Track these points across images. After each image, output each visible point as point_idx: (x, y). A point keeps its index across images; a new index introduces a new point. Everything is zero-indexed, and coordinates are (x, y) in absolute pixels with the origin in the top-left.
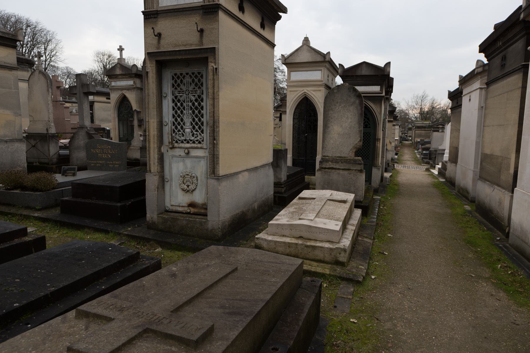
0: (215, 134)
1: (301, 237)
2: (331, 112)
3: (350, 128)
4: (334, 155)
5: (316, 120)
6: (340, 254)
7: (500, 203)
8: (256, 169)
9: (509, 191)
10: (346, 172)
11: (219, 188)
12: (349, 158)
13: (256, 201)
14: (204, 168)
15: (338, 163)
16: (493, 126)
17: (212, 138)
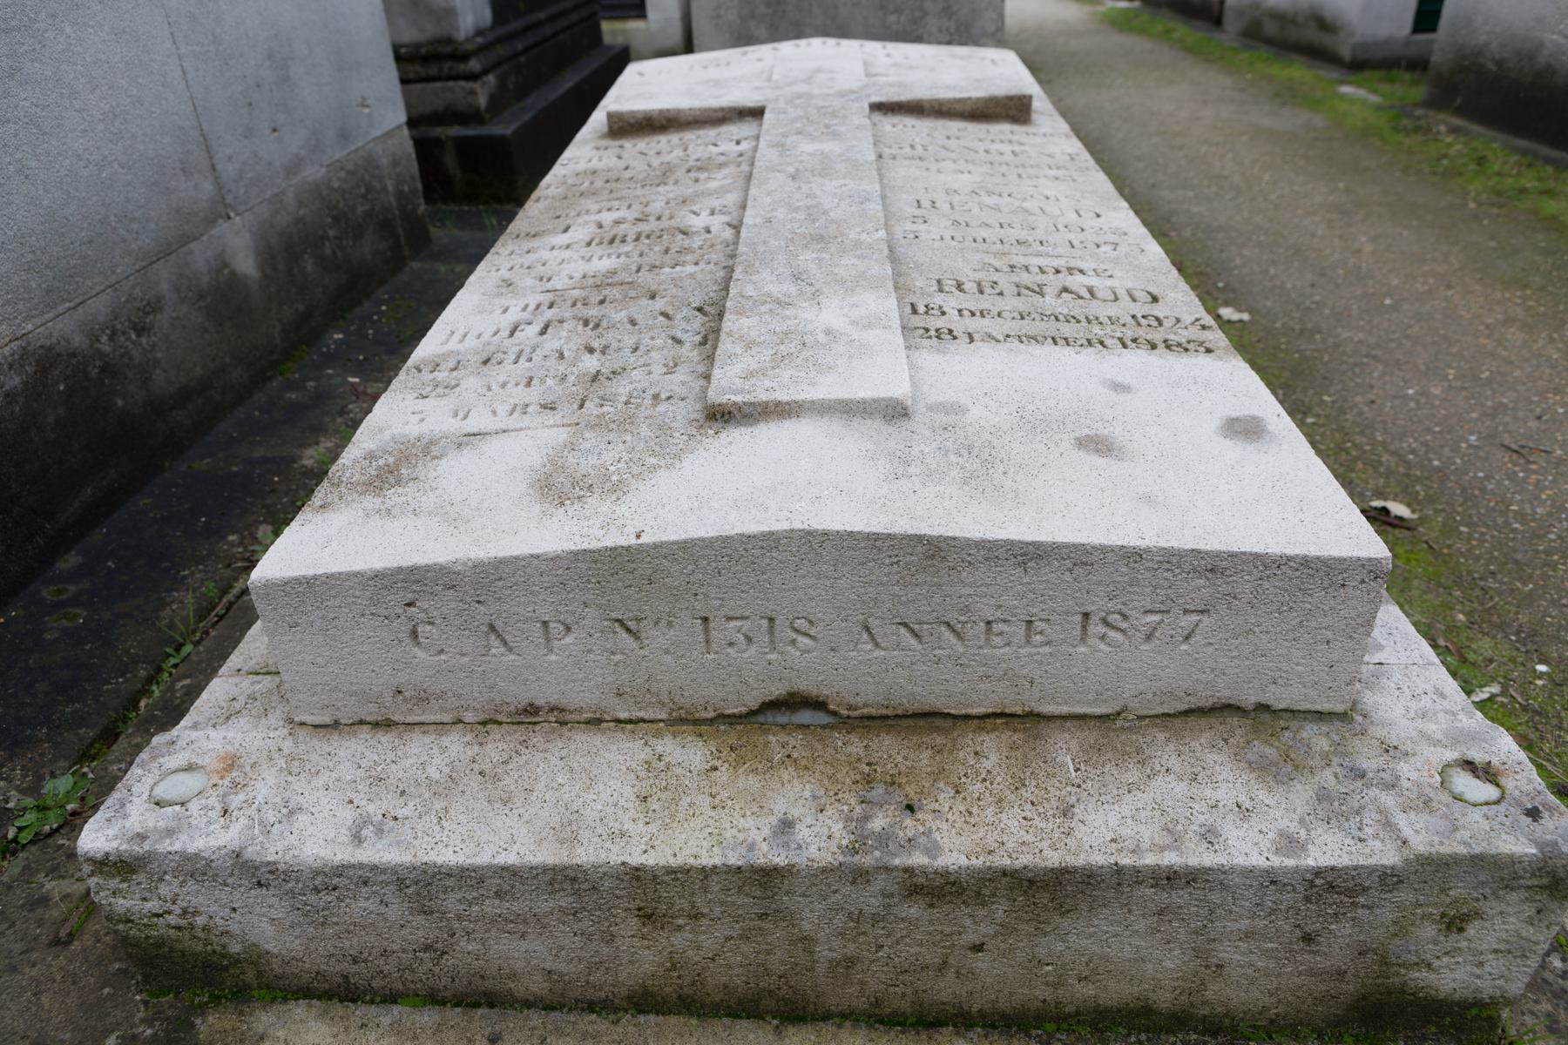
13: (220, 210)
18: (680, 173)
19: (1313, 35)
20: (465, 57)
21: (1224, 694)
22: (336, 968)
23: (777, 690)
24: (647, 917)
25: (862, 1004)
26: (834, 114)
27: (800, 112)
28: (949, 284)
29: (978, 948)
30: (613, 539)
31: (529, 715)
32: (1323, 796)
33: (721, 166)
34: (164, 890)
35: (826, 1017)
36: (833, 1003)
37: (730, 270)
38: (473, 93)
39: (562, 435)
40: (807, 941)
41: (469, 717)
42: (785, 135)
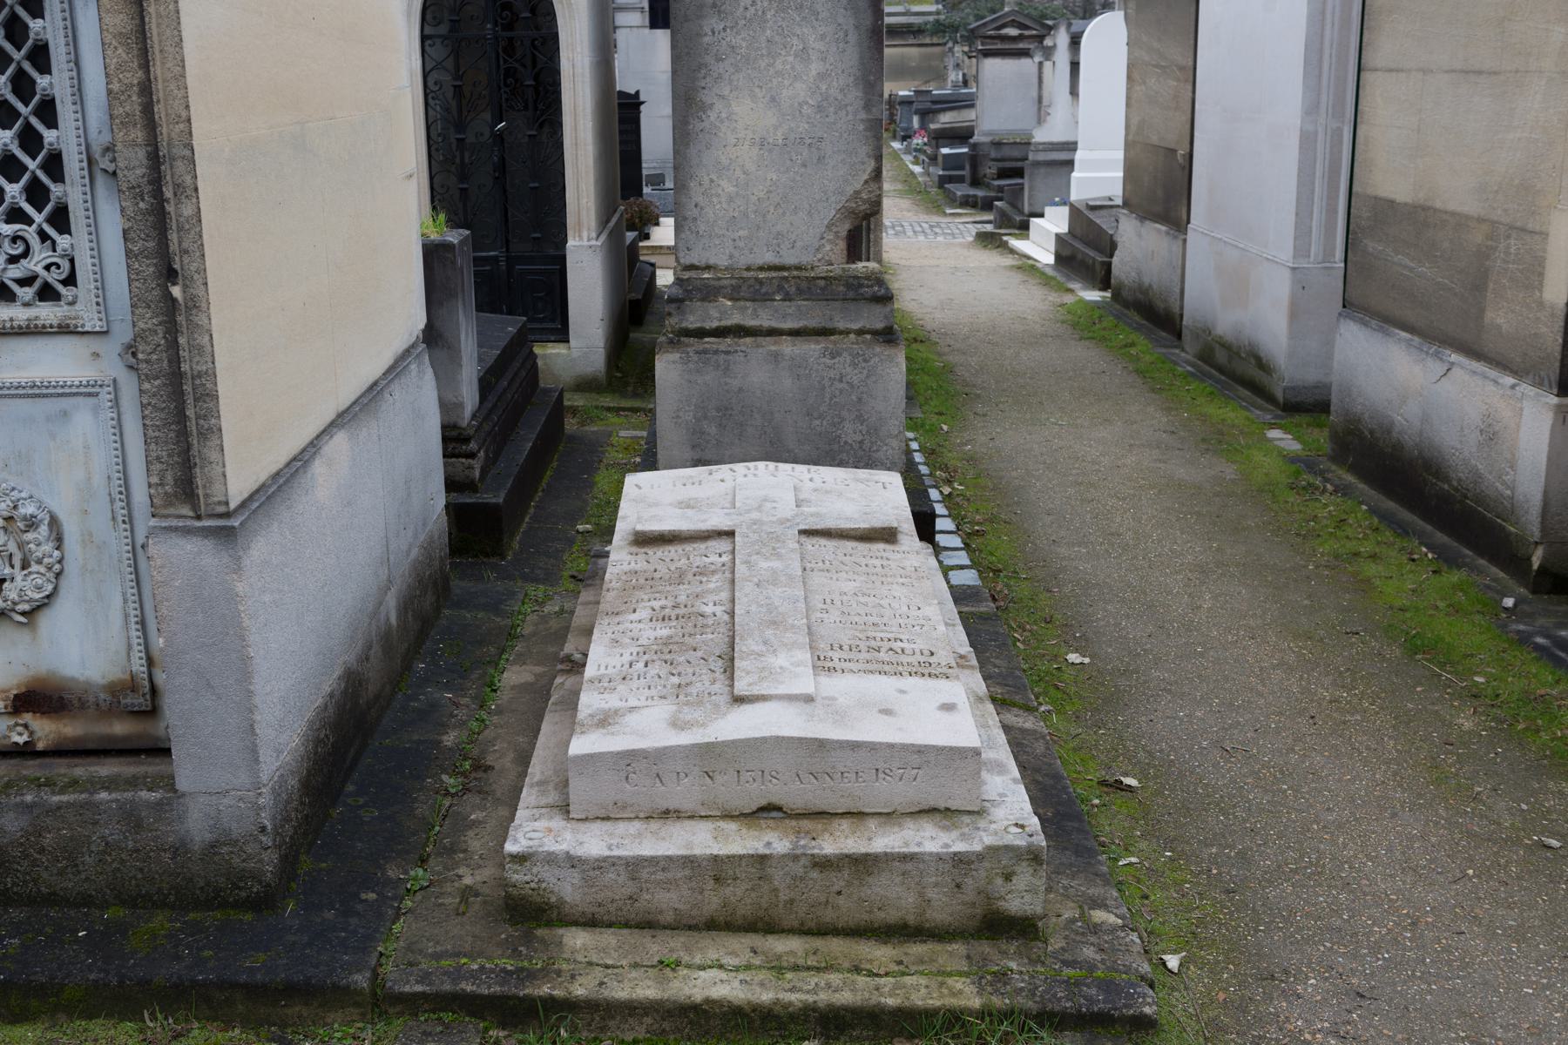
0: (173, 236)
1: (769, 811)
2: (712, 23)
3: (820, 108)
4: (743, 261)
5: (550, 43)
6: (1008, 877)
7: (1490, 435)
8: (373, 394)
9: (1538, 384)
10: (812, 349)
11: (240, 588)
12: (822, 270)
14: (101, 460)
15: (767, 298)
16: (1425, 71)
17: (149, 268)
18: (690, 576)
19: (1253, 372)
20: (467, 440)
21: (932, 803)
22: (590, 910)
23: (763, 802)
24: (717, 879)
25: (796, 924)
26: (778, 539)
27: (756, 536)
28: (836, 646)
29: (839, 893)
30: (706, 740)
31: (666, 814)
32: (963, 835)
33: (713, 572)
34: (535, 870)
35: (783, 931)
36: (786, 924)
37: (733, 637)
38: (471, 467)
39: (675, 708)
40: (776, 890)
41: (642, 815)
42: (750, 555)
